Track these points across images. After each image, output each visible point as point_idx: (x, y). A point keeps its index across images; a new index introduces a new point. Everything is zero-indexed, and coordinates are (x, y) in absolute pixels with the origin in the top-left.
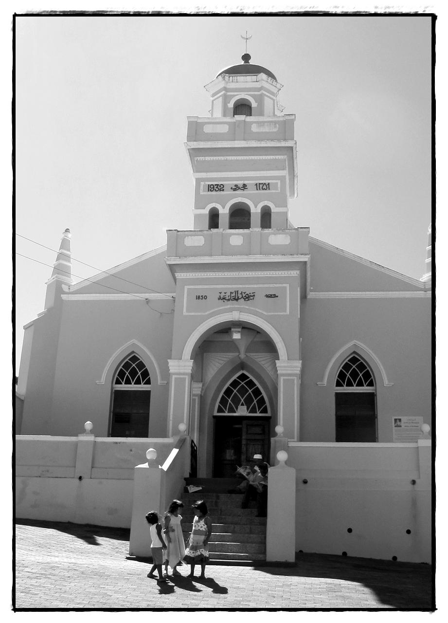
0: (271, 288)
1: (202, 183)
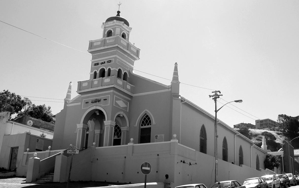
0: (104, 97)
1: (93, 63)
